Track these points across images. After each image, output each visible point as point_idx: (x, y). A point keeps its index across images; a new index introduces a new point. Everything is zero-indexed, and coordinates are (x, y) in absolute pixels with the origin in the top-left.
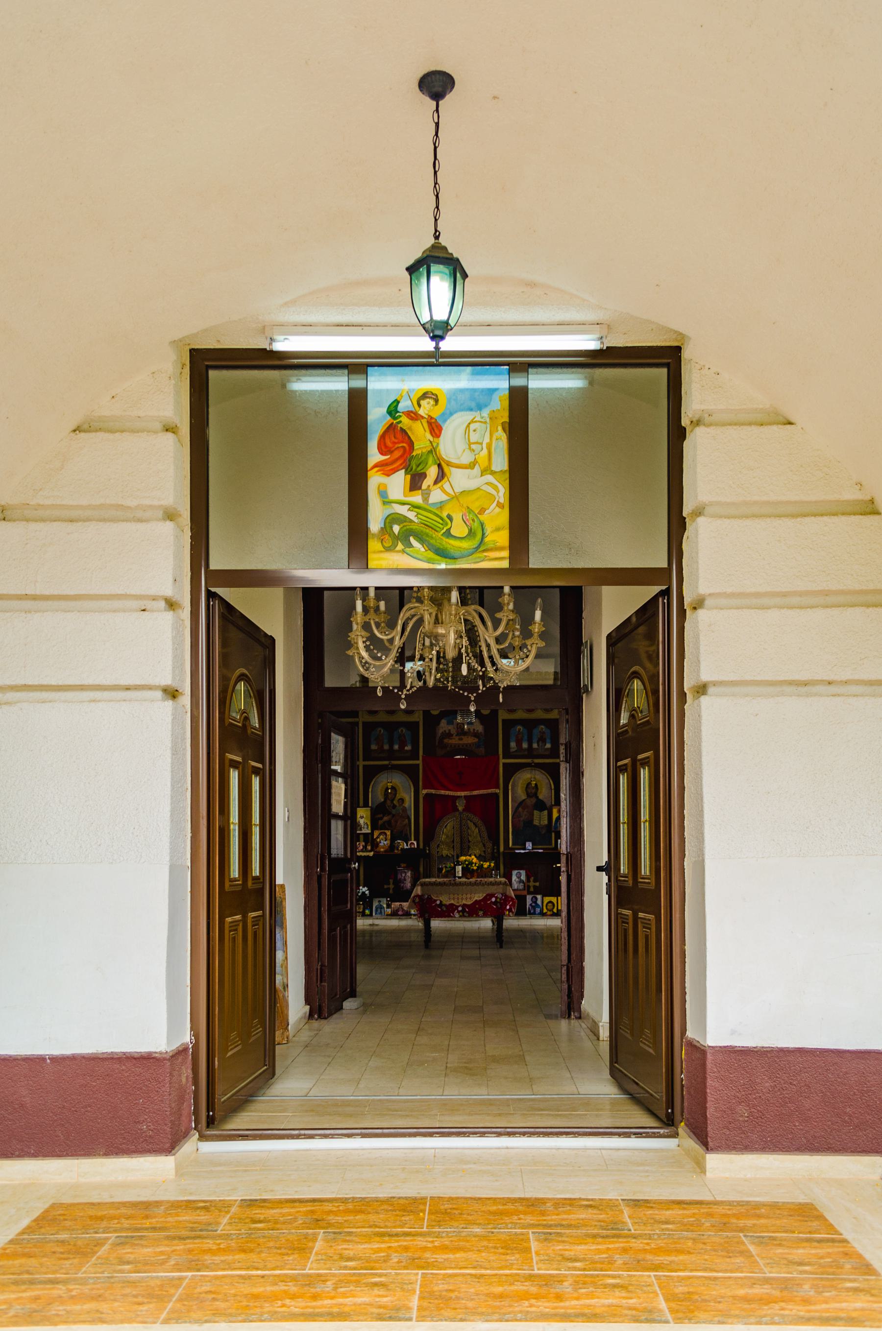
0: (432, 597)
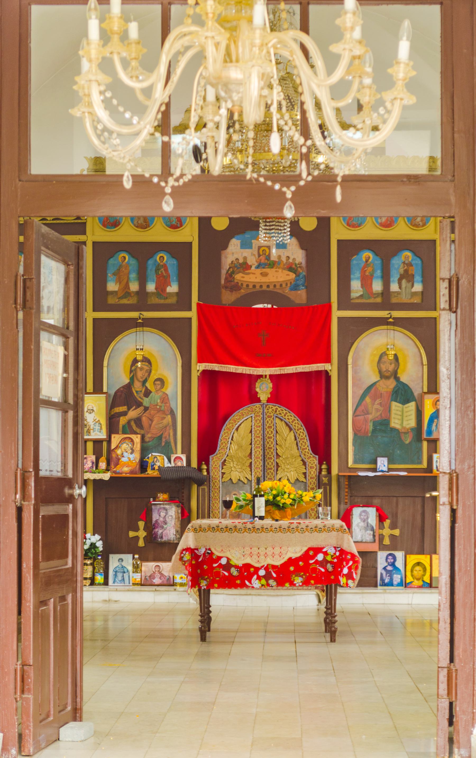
0: (220, 15)
